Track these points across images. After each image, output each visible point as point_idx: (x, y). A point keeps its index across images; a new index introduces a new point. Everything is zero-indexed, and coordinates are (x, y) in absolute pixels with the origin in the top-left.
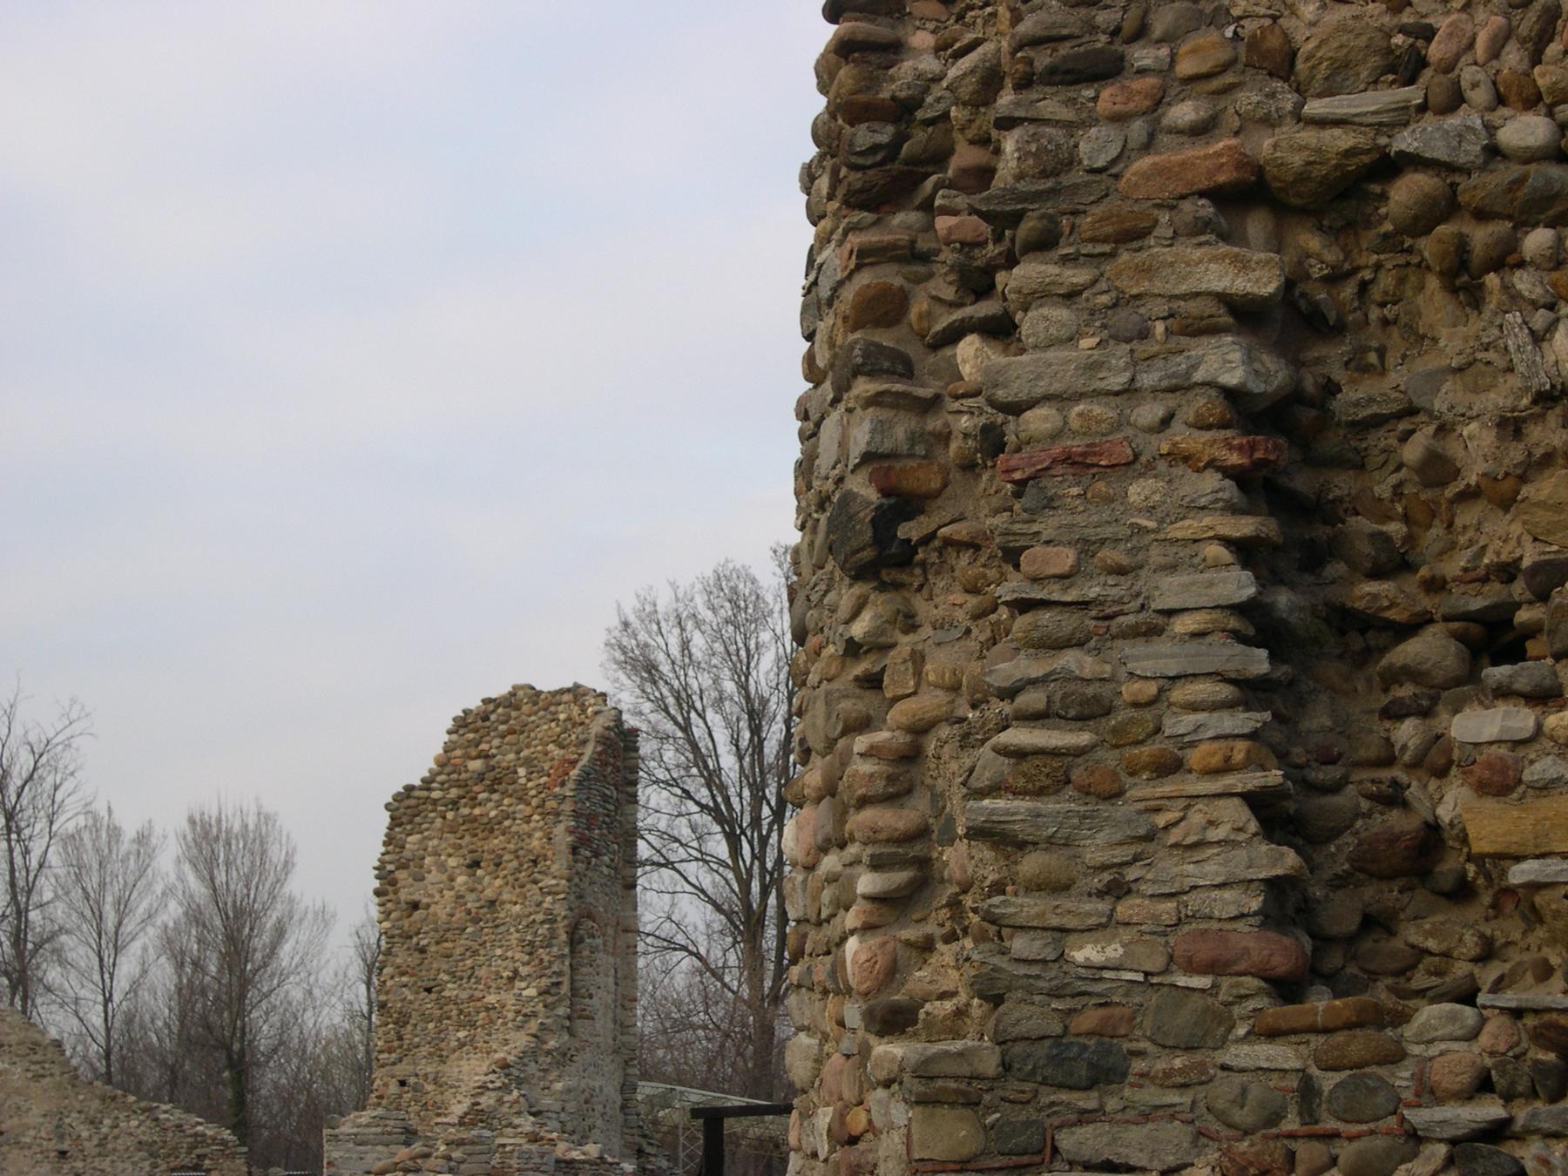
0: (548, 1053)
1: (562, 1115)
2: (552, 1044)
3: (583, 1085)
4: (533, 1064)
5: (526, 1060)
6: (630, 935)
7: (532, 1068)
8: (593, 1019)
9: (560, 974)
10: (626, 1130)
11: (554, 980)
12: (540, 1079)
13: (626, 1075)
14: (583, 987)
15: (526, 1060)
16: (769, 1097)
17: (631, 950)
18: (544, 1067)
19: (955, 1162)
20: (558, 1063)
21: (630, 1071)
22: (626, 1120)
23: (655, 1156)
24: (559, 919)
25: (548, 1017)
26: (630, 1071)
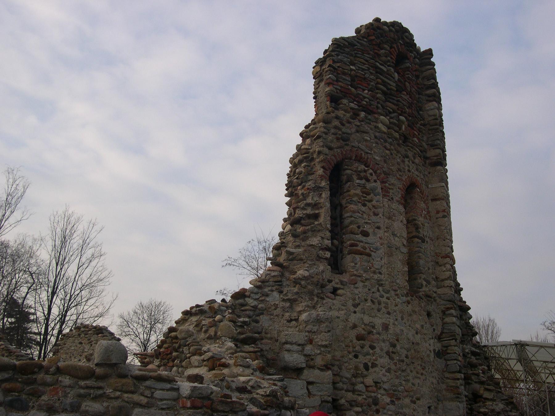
0: (296, 282)
1: (308, 348)
2: (301, 273)
3: (353, 318)
4: (275, 294)
5: (266, 290)
6: (438, 202)
7: (275, 297)
8: (369, 255)
9: (315, 206)
10: (447, 375)
11: (309, 211)
12: (284, 309)
13: (444, 324)
14: (351, 223)
15: (266, 290)
16: (413, 132)
17: (441, 214)
18: (290, 296)
19: (167, 400)
20: (311, 293)
21: (447, 320)
22: (447, 365)
23: (493, 400)
24: (315, 156)
25: (298, 246)
26: (447, 320)
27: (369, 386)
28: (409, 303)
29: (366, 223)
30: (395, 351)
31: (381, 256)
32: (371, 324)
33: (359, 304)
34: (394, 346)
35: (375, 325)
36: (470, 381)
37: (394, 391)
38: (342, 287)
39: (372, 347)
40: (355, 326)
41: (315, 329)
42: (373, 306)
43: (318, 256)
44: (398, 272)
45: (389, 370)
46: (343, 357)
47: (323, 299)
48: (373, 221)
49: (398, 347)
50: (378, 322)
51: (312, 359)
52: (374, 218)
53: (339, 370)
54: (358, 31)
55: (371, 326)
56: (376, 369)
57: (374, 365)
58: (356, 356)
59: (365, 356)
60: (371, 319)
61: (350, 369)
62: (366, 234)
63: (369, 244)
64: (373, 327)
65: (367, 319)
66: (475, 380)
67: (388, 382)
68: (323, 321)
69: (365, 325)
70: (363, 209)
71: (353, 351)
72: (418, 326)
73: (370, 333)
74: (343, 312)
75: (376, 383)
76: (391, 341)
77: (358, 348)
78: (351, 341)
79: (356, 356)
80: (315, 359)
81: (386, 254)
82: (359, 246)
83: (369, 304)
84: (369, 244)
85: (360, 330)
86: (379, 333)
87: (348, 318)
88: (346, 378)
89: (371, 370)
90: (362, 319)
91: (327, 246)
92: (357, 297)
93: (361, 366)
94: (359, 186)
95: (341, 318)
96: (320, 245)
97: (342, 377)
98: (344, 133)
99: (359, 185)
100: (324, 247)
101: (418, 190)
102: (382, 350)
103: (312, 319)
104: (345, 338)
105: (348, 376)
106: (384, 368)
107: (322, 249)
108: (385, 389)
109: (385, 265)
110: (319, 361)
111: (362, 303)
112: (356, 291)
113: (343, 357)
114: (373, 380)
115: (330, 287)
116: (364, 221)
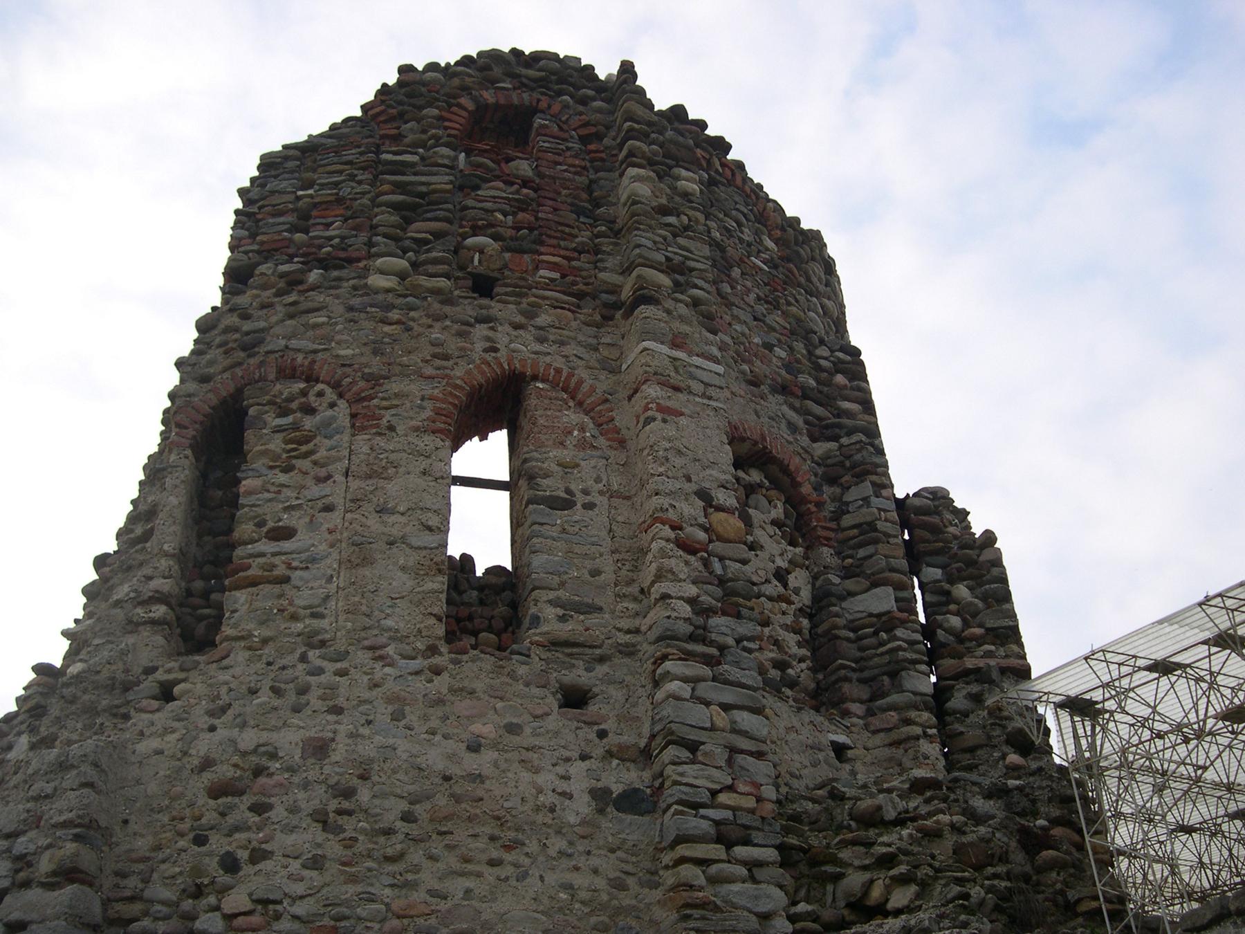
3: (204, 745)
27: (236, 916)
28: (437, 671)
29: (292, 508)
30: (353, 807)
31: (329, 572)
32: (263, 749)
33: (230, 705)
34: (348, 793)
35: (276, 748)
36: (829, 869)
37: (339, 919)
38: (181, 675)
39: (259, 809)
40: (207, 764)
41: (49, 788)
42: (276, 702)
43: (130, 622)
44: (392, 599)
45: (316, 863)
46: (158, 848)
47: (126, 717)
48: (309, 498)
49: (364, 795)
50: (289, 740)
51: (30, 865)
52: (315, 491)
53: (140, 886)
54: (678, 112)
55: (265, 753)
56: (267, 865)
57: (258, 856)
58: (200, 841)
59: (229, 835)
60: (265, 736)
61: (173, 877)
62: (284, 534)
63: (286, 554)
64: (273, 756)
65: (248, 739)
66: (857, 863)
67: (310, 895)
68: (75, 763)
69: (244, 754)
70: (282, 478)
71: (192, 829)
72: (485, 729)
73: (258, 772)
74: (172, 738)
75: (265, 902)
76: (332, 781)
77: (210, 817)
78: (191, 805)
79: (200, 841)
80: (38, 862)
81: (343, 567)
82: (254, 565)
83: (264, 697)
84: (286, 554)
85: (225, 771)
86: (291, 770)
87: (190, 748)
88: (163, 903)
89: (247, 870)
90: (233, 742)
91: (157, 591)
92: (224, 690)
93: (213, 865)
94: (278, 431)
95: (166, 753)
96: (132, 595)
97: (151, 901)
98: (247, 333)
99: (278, 430)
100: (146, 597)
101: (540, 385)
102: (293, 810)
103: (44, 767)
104: (173, 799)
105: (167, 894)
106: (296, 858)
107: (142, 603)
108: (295, 917)
109: (340, 592)
110: (45, 865)
111: (236, 705)
112: (224, 677)
113: (158, 848)
114: (250, 895)
115: (149, 685)
116: (281, 506)
